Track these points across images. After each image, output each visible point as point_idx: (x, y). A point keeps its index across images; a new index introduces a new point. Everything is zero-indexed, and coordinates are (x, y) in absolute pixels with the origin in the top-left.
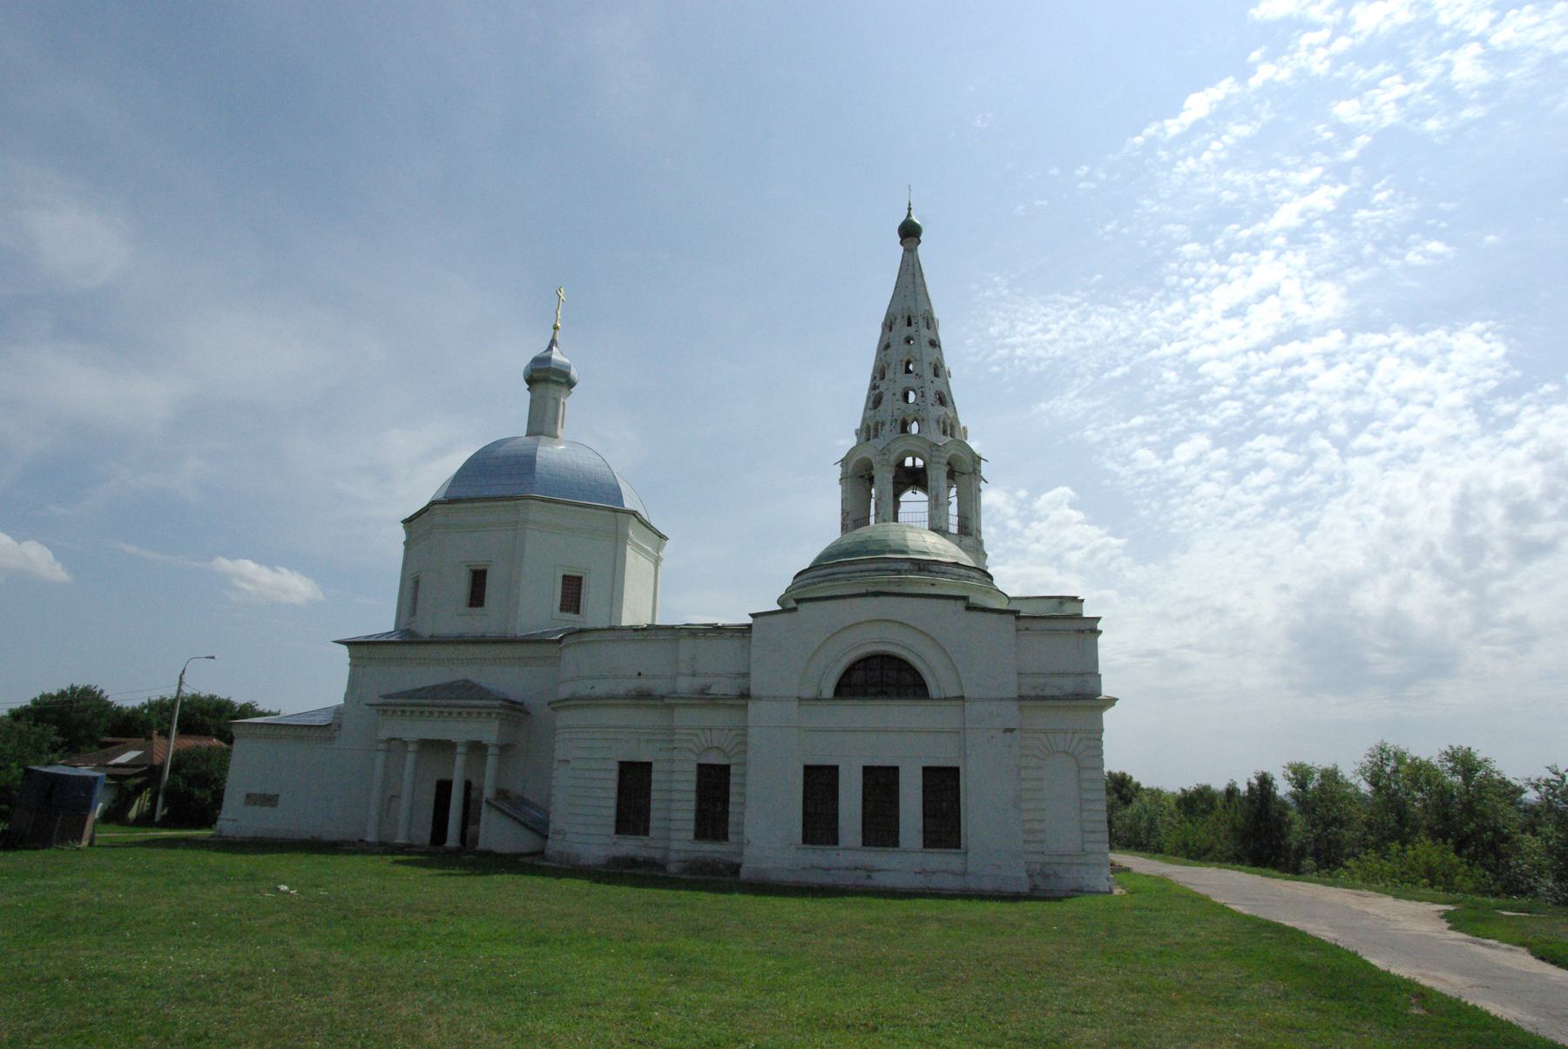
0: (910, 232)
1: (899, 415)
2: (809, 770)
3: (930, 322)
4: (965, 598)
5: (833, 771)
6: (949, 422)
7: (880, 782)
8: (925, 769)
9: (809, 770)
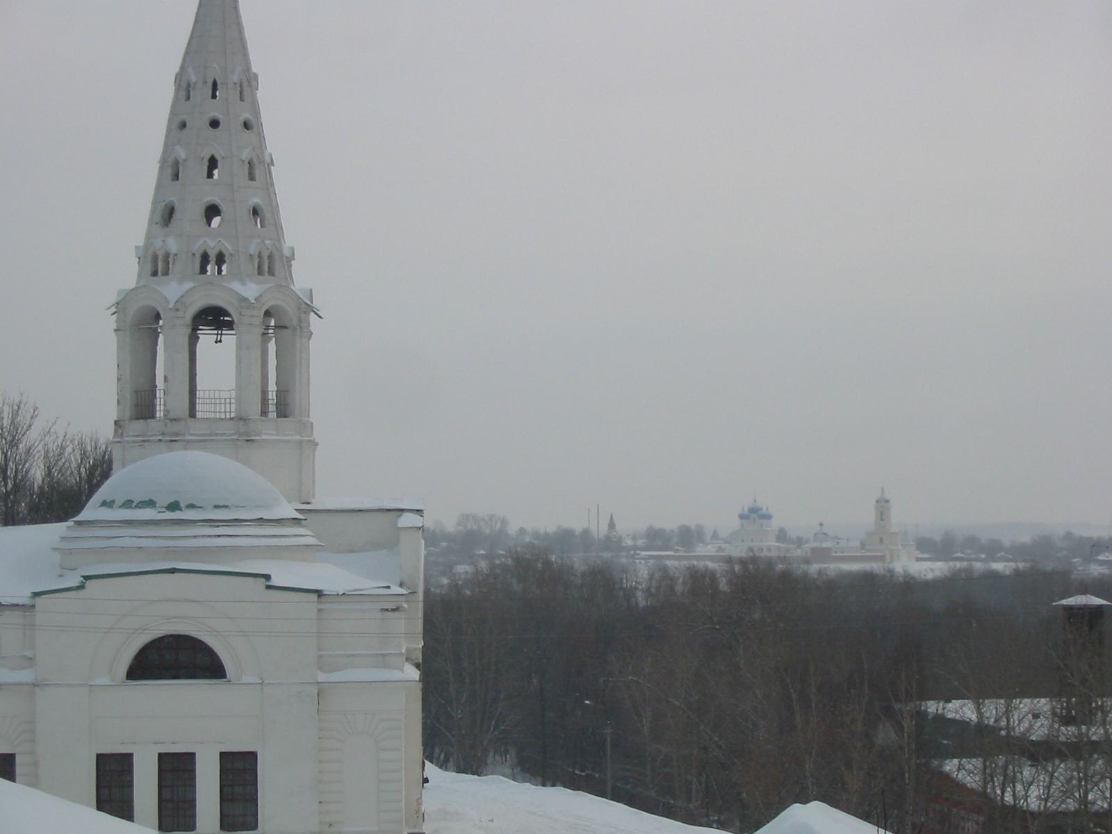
1: (198, 247)
3: (247, 86)
4: (268, 577)
5: (125, 761)
6: (265, 254)
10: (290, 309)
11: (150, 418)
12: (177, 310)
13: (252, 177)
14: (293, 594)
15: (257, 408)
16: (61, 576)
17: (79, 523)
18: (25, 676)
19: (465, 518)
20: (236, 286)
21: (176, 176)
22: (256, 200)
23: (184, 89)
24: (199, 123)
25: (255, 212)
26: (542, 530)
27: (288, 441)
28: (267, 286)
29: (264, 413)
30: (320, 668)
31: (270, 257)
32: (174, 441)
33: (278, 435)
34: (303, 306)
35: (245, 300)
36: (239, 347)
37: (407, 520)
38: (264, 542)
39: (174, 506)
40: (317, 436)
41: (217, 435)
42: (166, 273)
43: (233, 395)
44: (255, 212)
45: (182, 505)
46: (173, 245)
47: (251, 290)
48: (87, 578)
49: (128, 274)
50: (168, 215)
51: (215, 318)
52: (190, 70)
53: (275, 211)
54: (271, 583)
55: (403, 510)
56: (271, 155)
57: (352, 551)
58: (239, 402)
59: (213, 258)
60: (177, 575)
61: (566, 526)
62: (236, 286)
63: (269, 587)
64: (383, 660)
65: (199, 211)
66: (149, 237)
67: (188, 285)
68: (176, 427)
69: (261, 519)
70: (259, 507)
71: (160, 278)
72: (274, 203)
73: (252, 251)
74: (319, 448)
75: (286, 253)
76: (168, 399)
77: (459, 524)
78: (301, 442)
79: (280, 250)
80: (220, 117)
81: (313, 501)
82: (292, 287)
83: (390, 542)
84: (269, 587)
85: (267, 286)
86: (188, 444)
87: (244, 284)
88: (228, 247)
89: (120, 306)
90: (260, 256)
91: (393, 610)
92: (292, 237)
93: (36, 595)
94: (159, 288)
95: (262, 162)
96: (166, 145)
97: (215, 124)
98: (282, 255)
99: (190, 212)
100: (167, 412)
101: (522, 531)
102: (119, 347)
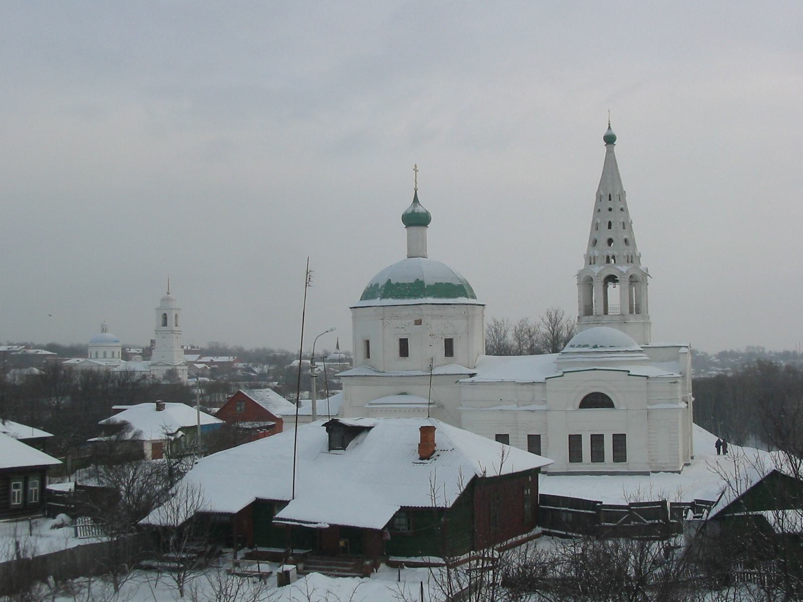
0: (610, 140)
1: (605, 254)
2: (401, 340)
3: (622, 195)
4: (629, 372)
5: (579, 437)
6: (629, 256)
7: (597, 440)
8: (613, 435)
9: (401, 340)
10: (639, 275)
11: (590, 315)
12: (598, 277)
13: (624, 228)
14: (637, 377)
15: (628, 311)
16: (557, 372)
17: (563, 353)
18: (544, 407)
19: (748, 348)
20: (619, 267)
21: (597, 229)
22: (626, 236)
23: (599, 198)
24: (604, 209)
25: (626, 240)
26: (778, 351)
27: (639, 323)
28: (630, 267)
29: (631, 312)
30: (648, 404)
31: (632, 257)
32: (598, 323)
33: (635, 320)
34: (644, 274)
35: (623, 272)
36: (621, 289)
37: (683, 350)
38: (622, 359)
39: (595, 347)
40: (651, 320)
41: (613, 321)
42: (594, 263)
43: (619, 306)
44: (626, 240)
45: (598, 346)
46: (596, 253)
47: (624, 268)
48: (564, 372)
49: (581, 264)
50: (594, 243)
51: (612, 279)
52: (601, 191)
53: (634, 240)
54: (629, 374)
55: (681, 347)
56: (631, 220)
57: (663, 362)
58: (621, 309)
59: (611, 257)
60: (596, 371)
61: (787, 350)
62: (619, 267)
63: (629, 375)
64: (671, 401)
65: (605, 241)
66: (588, 251)
67: (602, 267)
68: (599, 318)
69: (627, 351)
70: (626, 346)
71: (592, 265)
72: (633, 237)
73: (625, 255)
74: (652, 325)
75: (638, 255)
76: (598, 308)
77: (746, 350)
78: (644, 323)
79: (635, 254)
80: (612, 207)
81: (650, 344)
82: (640, 267)
83: (677, 359)
84: (629, 375)
85: (630, 267)
86: (603, 324)
87: (622, 266)
88: (616, 253)
89: (579, 275)
90: (628, 256)
91: (674, 383)
92: (640, 249)
93: (547, 378)
94: (592, 269)
95: (628, 222)
96: (593, 218)
97: (610, 210)
98: (636, 256)
99: (603, 241)
100: (595, 313)
101: (770, 352)
102: (579, 291)
